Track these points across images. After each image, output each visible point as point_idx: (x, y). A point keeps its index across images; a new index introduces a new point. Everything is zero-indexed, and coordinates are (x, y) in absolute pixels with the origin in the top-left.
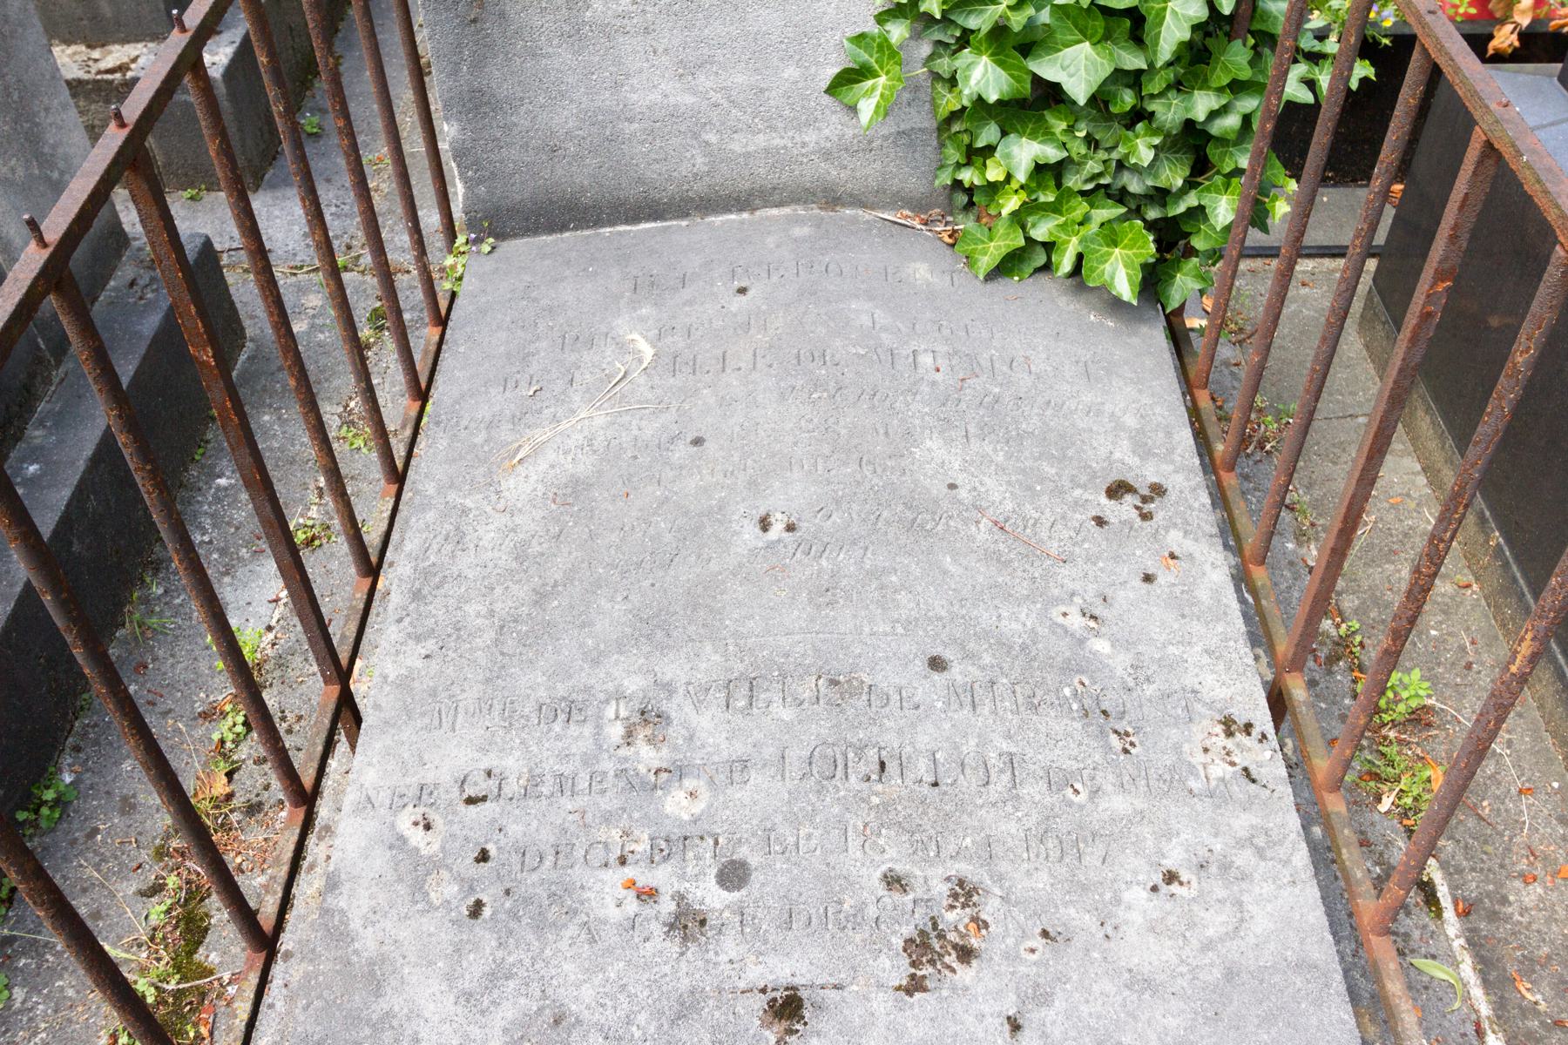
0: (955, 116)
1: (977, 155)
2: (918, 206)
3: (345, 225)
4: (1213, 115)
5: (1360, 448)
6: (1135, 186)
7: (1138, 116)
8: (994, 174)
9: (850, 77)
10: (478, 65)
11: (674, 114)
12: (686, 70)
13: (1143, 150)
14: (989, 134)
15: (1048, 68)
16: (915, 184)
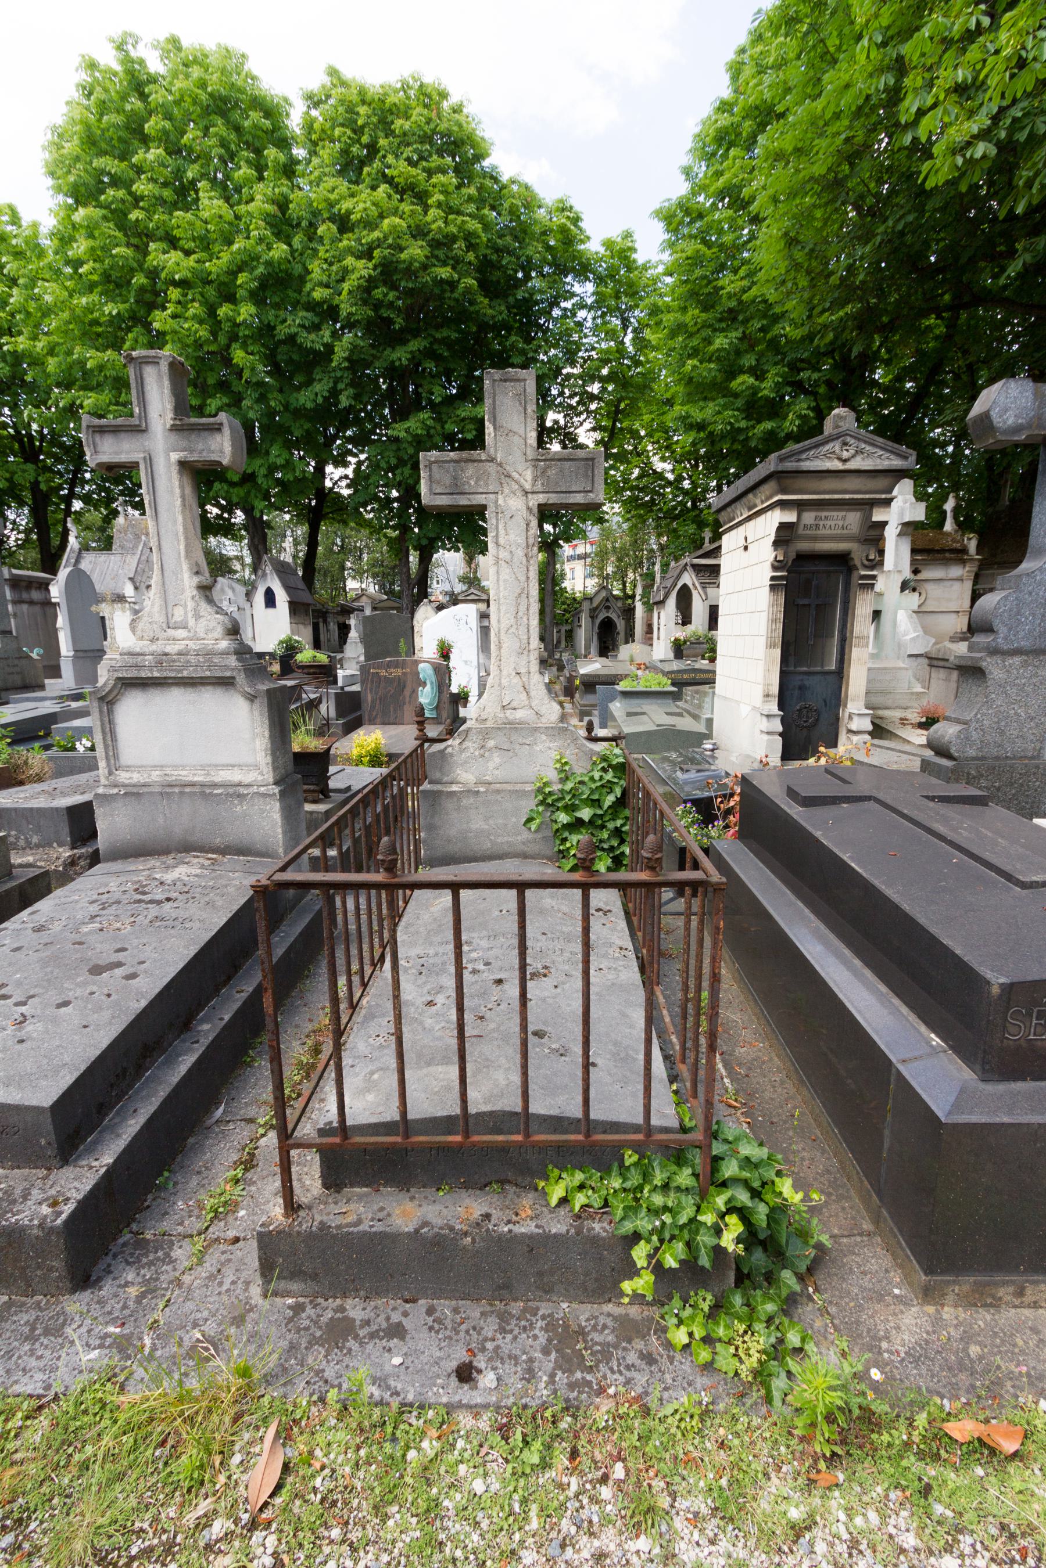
0: (557, 830)
1: (564, 840)
2: (550, 859)
3: (363, 906)
4: (622, 825)
5: (819, 1125)
6: (606, 846)
7: (603, 827)
8: (568, 845)
9: (530, 820)
10: (432, 817)
11: (482, 831)
12: (486, 819)
13: (605, 835)
14: (566, 834)
15: (578, 814)
16: (549, 853)
